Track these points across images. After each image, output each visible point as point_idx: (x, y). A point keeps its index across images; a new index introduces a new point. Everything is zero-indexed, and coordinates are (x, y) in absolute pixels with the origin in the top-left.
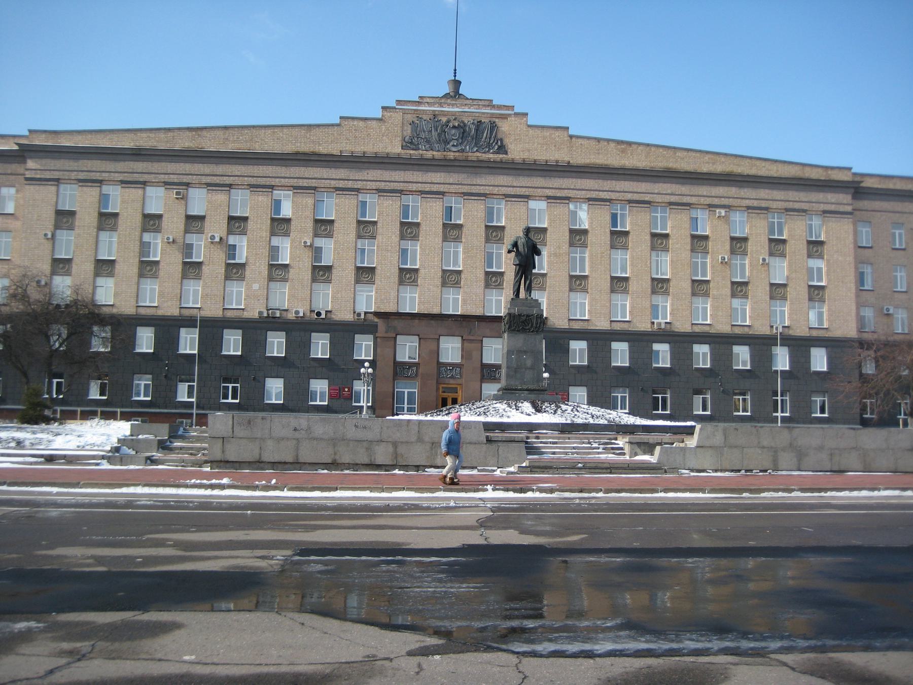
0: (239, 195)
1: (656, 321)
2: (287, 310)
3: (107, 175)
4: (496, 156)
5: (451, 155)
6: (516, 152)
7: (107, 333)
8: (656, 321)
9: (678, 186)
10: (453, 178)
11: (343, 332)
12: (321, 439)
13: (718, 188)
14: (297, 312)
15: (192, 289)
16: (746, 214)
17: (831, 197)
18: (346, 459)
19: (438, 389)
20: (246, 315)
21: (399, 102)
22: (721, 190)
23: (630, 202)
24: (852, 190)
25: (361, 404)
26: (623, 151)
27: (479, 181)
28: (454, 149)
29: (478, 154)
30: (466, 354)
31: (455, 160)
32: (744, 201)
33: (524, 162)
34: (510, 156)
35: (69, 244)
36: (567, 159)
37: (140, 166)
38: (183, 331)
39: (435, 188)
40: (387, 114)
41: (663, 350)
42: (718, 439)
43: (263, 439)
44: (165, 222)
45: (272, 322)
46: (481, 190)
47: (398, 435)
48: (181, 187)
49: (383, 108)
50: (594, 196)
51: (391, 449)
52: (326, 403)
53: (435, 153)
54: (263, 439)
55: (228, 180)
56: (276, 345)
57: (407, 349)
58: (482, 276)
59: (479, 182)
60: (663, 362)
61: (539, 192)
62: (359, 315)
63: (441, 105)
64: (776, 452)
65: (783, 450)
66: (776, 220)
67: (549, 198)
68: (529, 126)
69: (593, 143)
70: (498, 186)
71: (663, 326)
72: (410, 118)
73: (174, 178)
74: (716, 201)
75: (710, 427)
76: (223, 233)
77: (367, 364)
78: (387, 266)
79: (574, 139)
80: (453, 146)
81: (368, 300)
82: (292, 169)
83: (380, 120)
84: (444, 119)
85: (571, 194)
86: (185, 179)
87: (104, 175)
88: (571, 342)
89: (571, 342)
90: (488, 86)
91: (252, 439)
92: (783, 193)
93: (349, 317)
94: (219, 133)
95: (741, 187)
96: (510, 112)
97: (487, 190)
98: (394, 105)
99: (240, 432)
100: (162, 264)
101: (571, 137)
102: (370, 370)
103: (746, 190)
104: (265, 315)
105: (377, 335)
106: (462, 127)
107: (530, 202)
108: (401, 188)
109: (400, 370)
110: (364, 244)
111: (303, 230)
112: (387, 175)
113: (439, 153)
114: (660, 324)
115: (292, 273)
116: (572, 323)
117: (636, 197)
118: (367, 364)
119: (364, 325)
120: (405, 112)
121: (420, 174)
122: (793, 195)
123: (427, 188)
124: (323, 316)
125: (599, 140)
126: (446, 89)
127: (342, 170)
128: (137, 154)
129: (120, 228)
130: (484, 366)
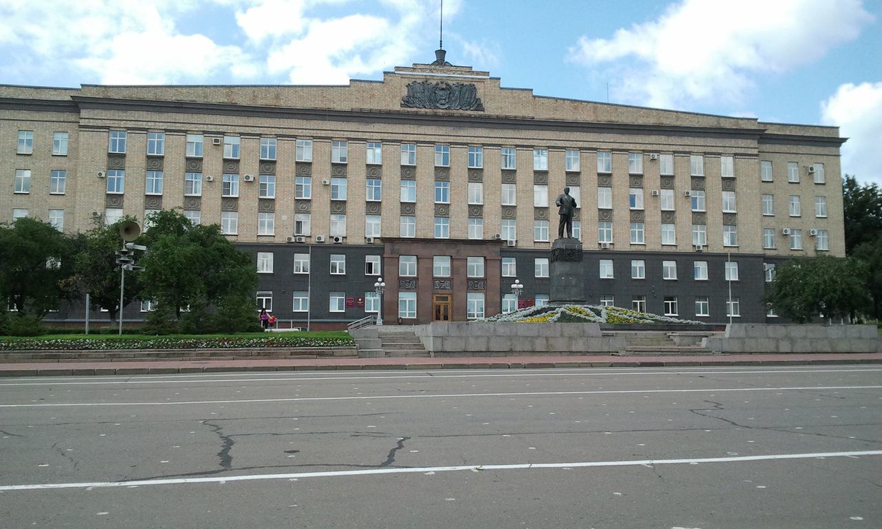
0: (267, 143)
5: (440, 112)
6: (491, 109)
7: (270, 256)
9: (619, 136)
10: (442, 130)
11: (355, 254)
12: (503, 336)
13: (651, 137)
14: (319, 238)
15: (229, 219)
16: (579, 152)
17: (741, 142)
18: (518, 348)
19: (433, 299)
24: (758, 137)
27: (462, 133)
28: (441, 106)
29: (461, 111)
30: (453, 270)
31: (443, 116)
32: (671, 147)
33: (498, 118)
34: (486, 113)
35: (123, 183)
36: (531, 115)
37: (181, 117)
38: (260, 255)
39: (428, 139)
40: (388, 78)
41: (670, 265)
44: (205, 164)
45: (338, 247)
46: (464, 140)
47: (549, 332)
48: (651, 155)
49: (385, 73)
50: (553, 145)
51: (545, 342)
52: (343, 311)
53: (427, 110)
55: (258, 131)
56: (302, 262)
57: (408, 266)
60: (672, 276)
61: (729, 150)
62: (369, 239)
63: (431, 71)
64: (778, 341)
65: (783, 339)
68: (501, 88)
69: (553, 101)
70: (477, 137)
72: (406, 82)
73: (212, 128)
74: (649, 147)
75: (736, 325)
76: (256, 175)
79: (537, 98)
80: (442, 104)
81: (374, 228)
82: (312, 122)
83: (383, 83)
84: (434, 82)
86: (221, 129)
87: (149, 124)
88: (664, 262)
89: (664, 262)
90: (473, 54)
91: (461, 337)
92: (702, 139)
93: (361, 242)
95: (668, 135)
96: (486, 77)
100: (203, 199)
101: (534, 97)
103: (673, 138)
105: (384, 256)
106: (449, 88)
107: (692, 157)
108: (401, 139)
109: (405, 284)
110: (303, 182)
111: (322, 173)
113: (430, 110)
114: (605, 244)
115: (314, 206)
116: (259, 238)
118: (380, 279)
119: (371, 248)
120: (403, 77)
123: (422, 138)
124: (340, 241)
125: (556, 99)
127: (592, 134)
129: (165, 169)
130: (400, 279)
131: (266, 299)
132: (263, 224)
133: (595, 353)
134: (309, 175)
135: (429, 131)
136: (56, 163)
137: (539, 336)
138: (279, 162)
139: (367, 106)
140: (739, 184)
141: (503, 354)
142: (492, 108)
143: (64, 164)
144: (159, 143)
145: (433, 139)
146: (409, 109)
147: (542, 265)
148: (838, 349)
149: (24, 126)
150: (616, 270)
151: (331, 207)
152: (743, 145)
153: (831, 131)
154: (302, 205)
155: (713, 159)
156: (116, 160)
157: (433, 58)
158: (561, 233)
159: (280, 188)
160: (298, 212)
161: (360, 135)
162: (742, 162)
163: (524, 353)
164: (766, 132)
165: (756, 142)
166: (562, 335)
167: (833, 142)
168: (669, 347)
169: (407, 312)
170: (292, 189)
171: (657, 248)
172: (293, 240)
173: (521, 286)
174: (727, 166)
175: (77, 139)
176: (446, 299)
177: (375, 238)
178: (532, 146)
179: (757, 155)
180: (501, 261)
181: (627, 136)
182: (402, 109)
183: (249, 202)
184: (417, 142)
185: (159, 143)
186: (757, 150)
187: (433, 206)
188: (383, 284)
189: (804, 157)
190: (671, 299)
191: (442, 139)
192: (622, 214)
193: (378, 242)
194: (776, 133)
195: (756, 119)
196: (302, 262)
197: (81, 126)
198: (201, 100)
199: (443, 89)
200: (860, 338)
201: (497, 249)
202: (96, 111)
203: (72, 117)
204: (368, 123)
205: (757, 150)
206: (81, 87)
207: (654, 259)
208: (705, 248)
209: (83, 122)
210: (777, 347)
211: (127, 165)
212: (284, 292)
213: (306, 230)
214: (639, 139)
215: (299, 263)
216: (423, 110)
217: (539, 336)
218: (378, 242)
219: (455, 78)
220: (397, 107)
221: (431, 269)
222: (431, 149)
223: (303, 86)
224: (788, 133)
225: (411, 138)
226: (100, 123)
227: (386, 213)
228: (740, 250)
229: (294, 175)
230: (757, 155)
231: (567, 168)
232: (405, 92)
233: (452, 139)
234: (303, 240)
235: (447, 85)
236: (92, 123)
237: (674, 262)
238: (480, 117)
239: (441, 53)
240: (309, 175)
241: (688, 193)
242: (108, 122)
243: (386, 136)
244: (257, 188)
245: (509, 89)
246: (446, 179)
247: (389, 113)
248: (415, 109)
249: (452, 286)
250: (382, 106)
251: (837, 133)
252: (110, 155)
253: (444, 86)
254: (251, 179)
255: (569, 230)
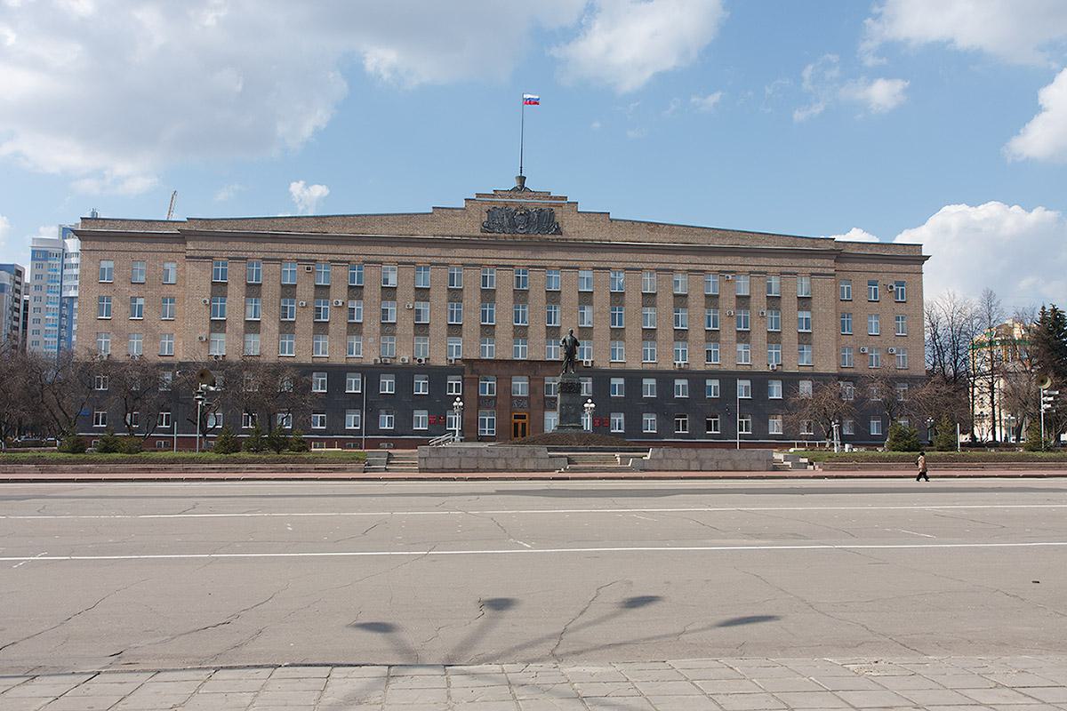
1: (677, 362)
2: (395, 358)
3: (251, 253)
4: (553, 237)
7: (748, 383)
8: (677, 362)
11: (437, 375)
17: (817, 262)
19: (511, 417)
20: (364, 362)
21: (478, 195)
22: (729, 259)
23: (657, 270)
24: (835, 257)
25: (453, 428)
26: (652, 230)
28: (521, 232)
30: (532, 390)
39: (507, 262)
41: (714, 383)
42: (660, 455)
43: (444, 458)
45: (425, 369)
48: (310, 264)
54: (444, 458)
56: (387, 385)
57: (488, 386)
58: (544, 330)
59: (540, 257)
66: (220, 268)
67: (594, 268)
71: (682, 366)
72: (486, 207)
73: (304, 256)
74: (725, 268)
77: (590, 401)
78: (471, 320)
83: (464, 209)
85: (612, 265)
89: (676, 381)
91: (439, 458)
93: (444, 363)
94: (858, 245)
97: (546, 263)
98: (475, 197)
99: (433, 455)
101: (611, 220)
102: (461, 404)
104: (379, 362)
106: (528, 213)
109: (483, 403)
111: (406, 296)
112: (470, 252)
114: (680, 365)
115: (399, 329)
116: (612, 365)
117: (662, 266)
118: (458, 399)
121: (495, 251)
122: (786, 261)
123: (501, 262)
124: (453, 362)
126: (515, 184)
128: (275, 238)
134: (394, 299)
137: (499, 458)
138: (366, 287)
144: (258, 271)
147: (806, 387)
148: (739, 468)
149: (137, 256)
154: (388, 329)
155: (790, 279)
156: (219, 289)
157: (515, 184)
159: (364, 311)
162: (818, 280)
166: (517, 457)
169: (487, 429)
170: (378, 313)
171: (732, 368)
173: (593, 405)
174: (803, 287)
175: (184, 268)
176: (524, 417)
178: (609, 269)
179: (834, 275)
183: (338, 325)
187: (512, 328)
191: (521, 263)
192: (665, 334)
196: (387, 385)
200: (759, 459)
203: (180, 248)
204: (449, 248)
210: (689, 465)
211: (229, 292)
214: (715, 259)
217: (499, 458)
219: (532, 204)
221: (509, 389)
223: (388, 215)
230: (834, 275)
233: (530, 263)
237: (686, 381)
240: (394, 299)
241: (763, 313)
245: (449, 209)
246: (525, 302)
249: (529, 404)
254: (340, 304)
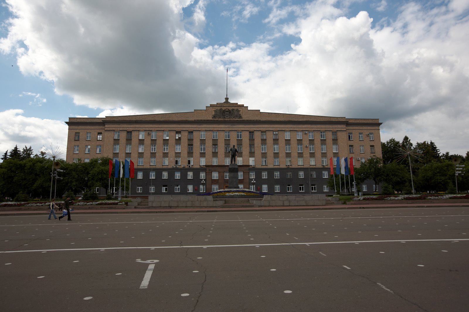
10: (227, 126)
18: (181, 205)
28: (227, 118)
33: (247, 121)
36: (259, 119)
39: (222, 129)
46: (235, 129)
55: (163, 129)
60: (253, 177)
62: (201, 166)
73: (147, 129)
74: (304, 129)
82: (142, 125)
86: (151, 129)
93: (198, 167)
105: (206, 172)
123: (220, 129)
131: (153, 188)
132: (152, 161)
133: (210, 207)
135: (222, 126)
136: (98, 143)
139: (200, 119)
140: (112, 142)
141: (175, 207)
142: (245, 117)
143: (101, 143)
145: (224, 129)
146: (215, 119)
150: (268, 175)
151: (188, 154)
152: (340, 127)
153: (377, 120)
158: (232, 162)
160: (176, 157)
161: (198, 129)
163: (207, 207)
164: (349, 122)
165: (345, 126)
166: (198, 200)
167: (87, 124)
168: (248, 204)
172: (174, 167)
177: (203, 165)
179: (346, 131)
180: (249, 172)
181: (296, 125)
182: (212, 119)
184: (218, 131)
185: (216, 135)
186: (346, 129)
188: (255, 182)
189: (365, 131)
190: (302, 185)
191: (227, 129)
193: (204, 167)
194: (353, 122)
195: (345, 117)
197: (105, 130)
198: (143, 120)
199: (227, 111)
201: (248, 168)
202: (110, 125)
205: (346, 129)
206: (105, 117)
207: (159, 172)
208: (327, 166)
209: (106, 129)
210: (283, 204)
211: (120, 143)
212: (171, 185)
213: (192, 164)
214: (300, 126)
215: (164, 175)
216: (220, 119)
218: (204, 167)
220: (211, 119)
222: (223, 133)
224: (358, 122)
225: (216, 129)
226: (111, 129)
227: (207, 156)
228: (328, 166)
229: (175, 144)
230: (346, 131)
231: (285, 138)
232: (214, 113)
233: (231, 129)
234: (178, 167)
235: (229, 109)
236: (109, 129)
238: (241, 121)
239: (227, 99)
242: (114, 128)
243: (207, 129)
244: (309, 149)
247: (208, 120)
248: (217, 119)
250: (205, 118)
251: (378, 121)
252: (274, 140)
253: (227, 110)
255: (235, 161)
